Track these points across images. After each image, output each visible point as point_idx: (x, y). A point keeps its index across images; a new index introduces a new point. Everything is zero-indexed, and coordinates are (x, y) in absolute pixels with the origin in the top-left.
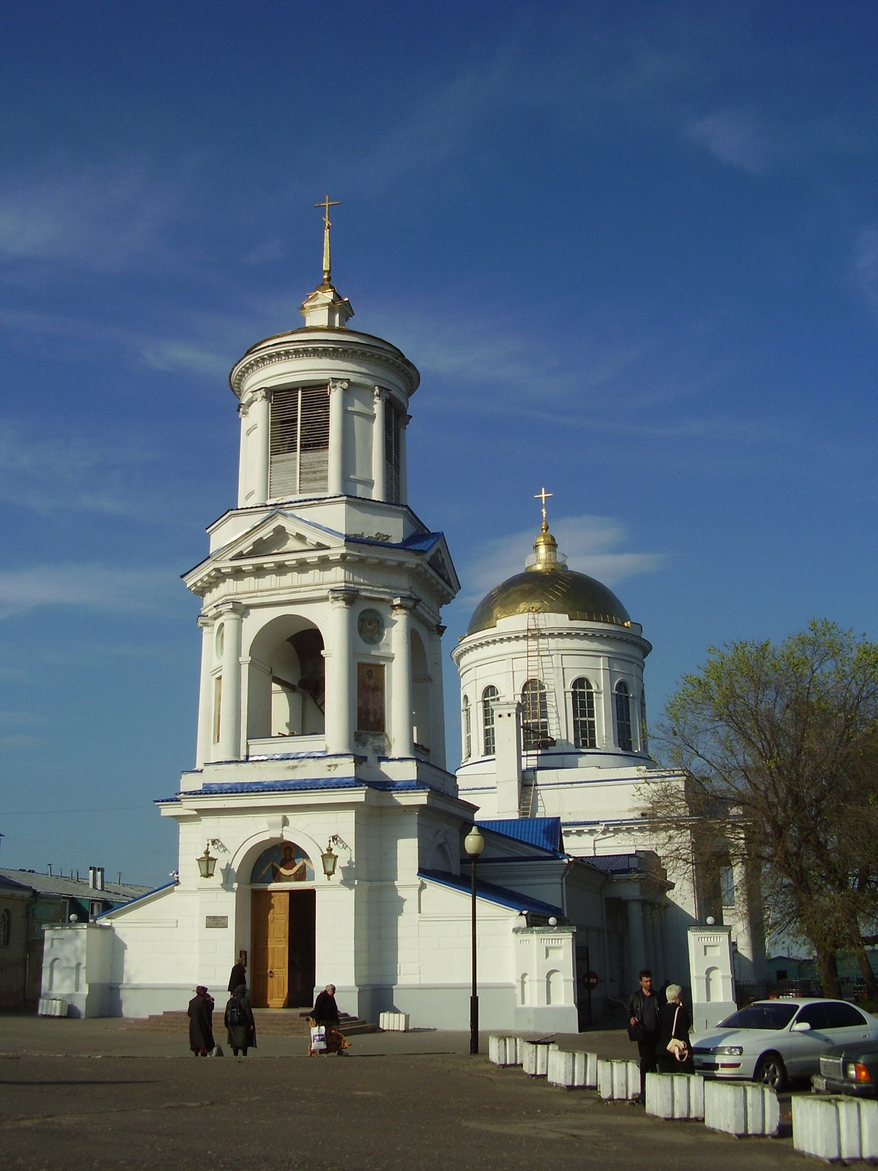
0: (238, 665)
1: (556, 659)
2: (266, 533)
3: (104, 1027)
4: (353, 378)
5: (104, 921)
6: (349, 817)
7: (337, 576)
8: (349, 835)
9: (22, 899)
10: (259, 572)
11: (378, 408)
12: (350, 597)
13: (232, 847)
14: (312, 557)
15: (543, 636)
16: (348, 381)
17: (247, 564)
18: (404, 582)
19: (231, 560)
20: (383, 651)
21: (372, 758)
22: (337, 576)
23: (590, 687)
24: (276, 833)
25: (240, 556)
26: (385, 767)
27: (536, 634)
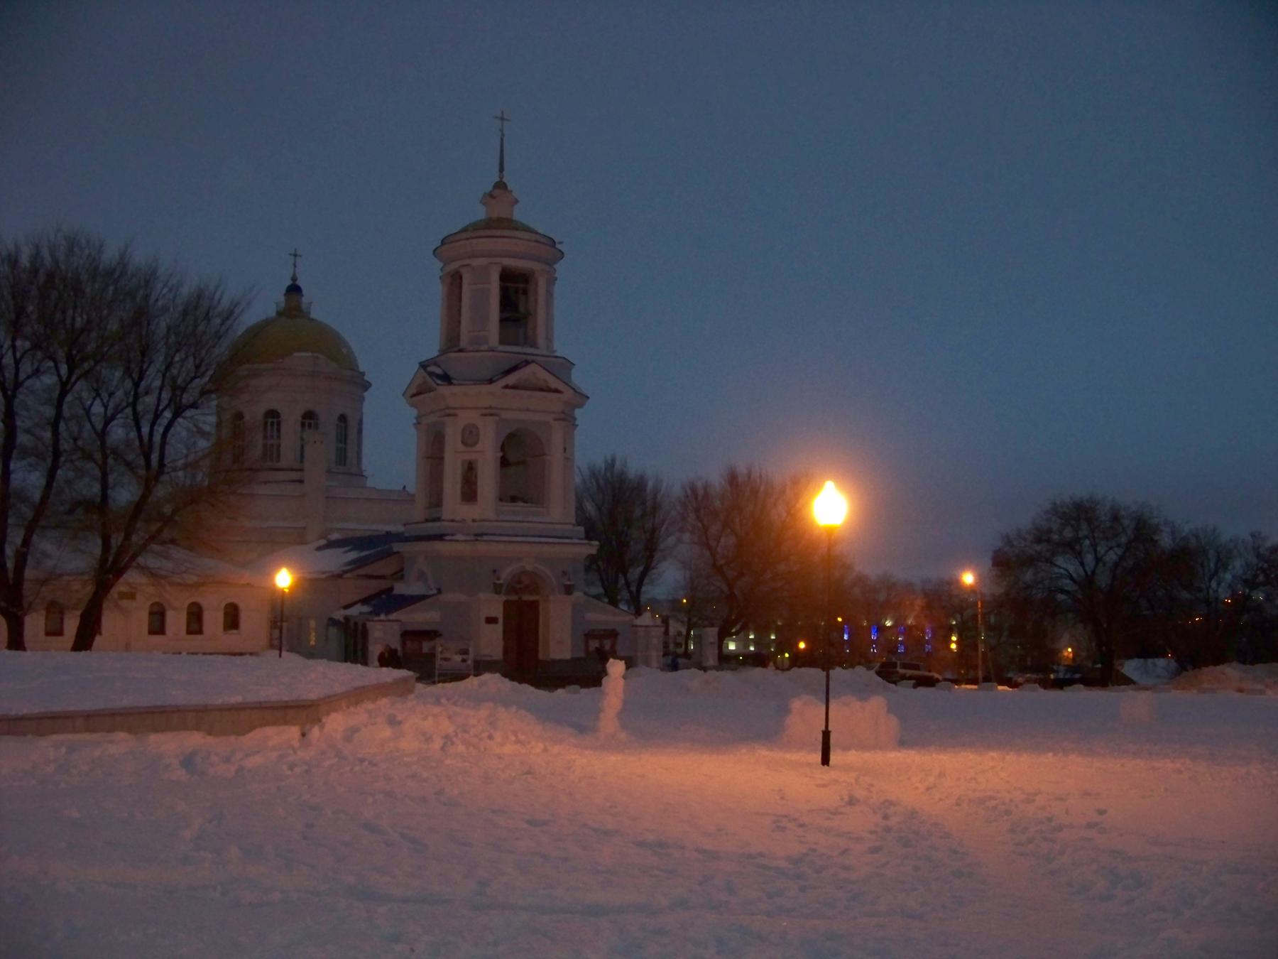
25: (507, 387)
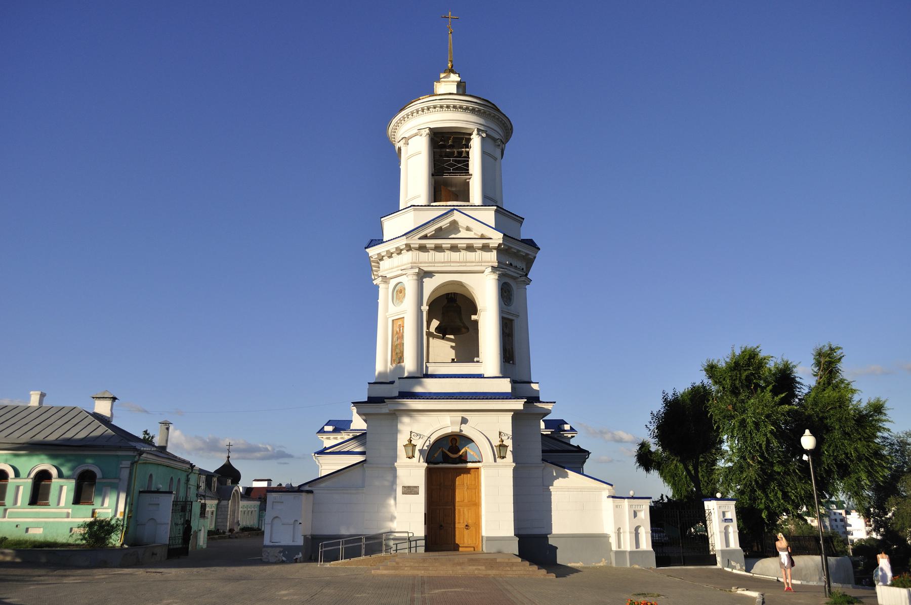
2: (444, 223)
3: (442, 566)
6: (508, 417)
8: (508, 429)
10: (438, 248)
14: (479, 243)
17: (430, 243)
19: (419, 239)
24: (456, 429)
25: (425, 237)
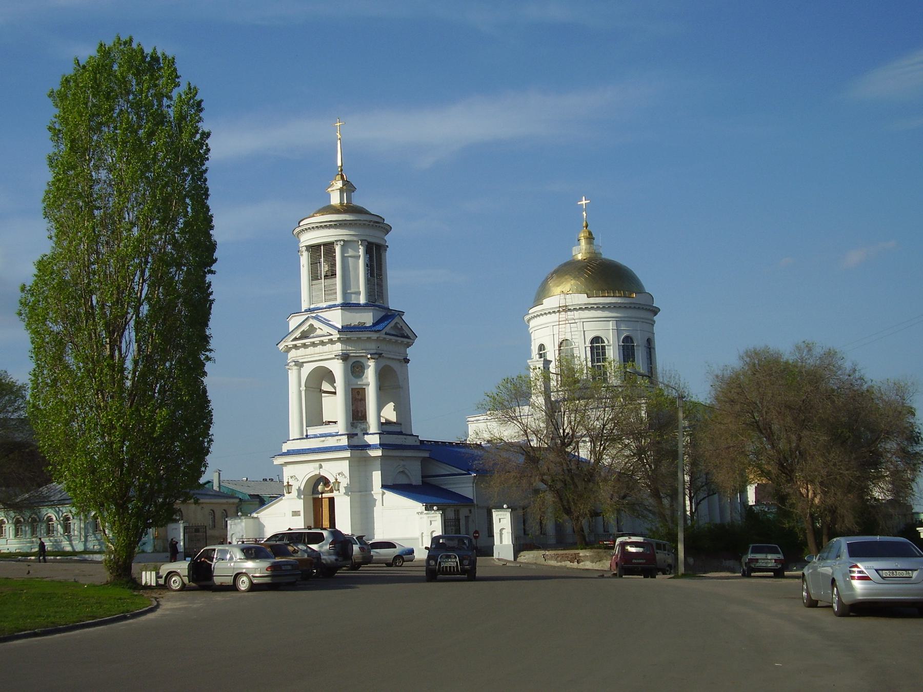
0: (300, 392)
1: (580, 325)
2: (305, 327)
4: (346, 238)
5: (255, 515)
7: (338, 348)
9: (233, 504)
10: (305, 346)
11: (361, 251)
12: (345, 357)
13: (300, 479)
15: (569, 310)
16: (344, 241)
18: (373, 347)
20: (364, 381)
21: (360, 434)
22: (338, 348)
23: (603, 342)
25: (296, 339)
26: (367, 438)
27: (566, 309)
